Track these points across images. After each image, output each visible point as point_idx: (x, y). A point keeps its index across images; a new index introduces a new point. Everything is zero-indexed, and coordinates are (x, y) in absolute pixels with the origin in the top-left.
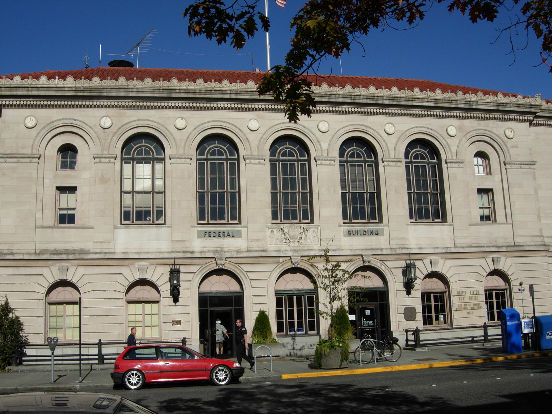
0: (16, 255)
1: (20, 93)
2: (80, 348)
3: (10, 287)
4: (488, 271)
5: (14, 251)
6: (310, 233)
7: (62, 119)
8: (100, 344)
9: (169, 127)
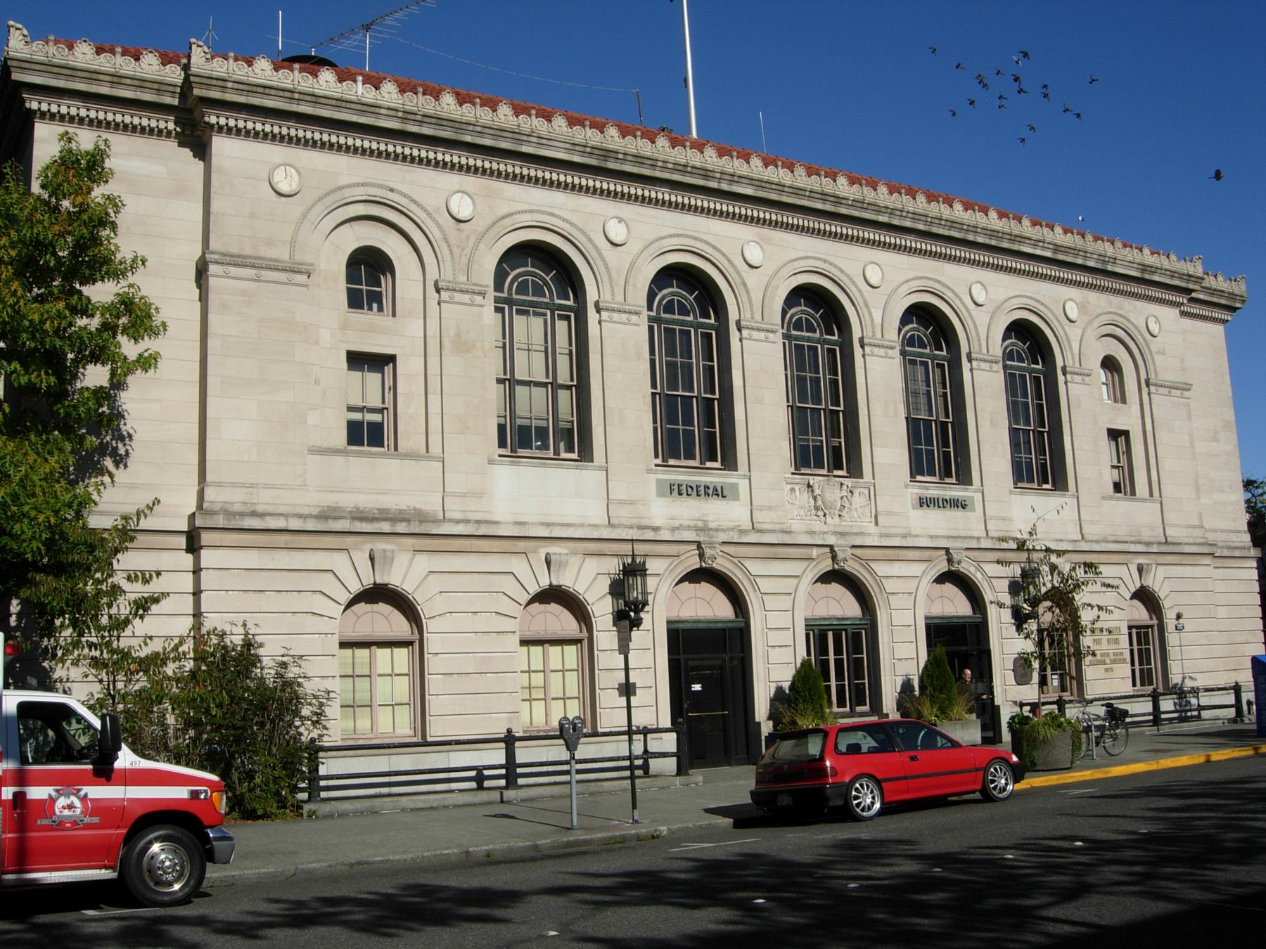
0: (268, 518)
1: (269, 103)
2: (630, 741)
3: (253, 602)
4: (534, 589)
5: (260, 509)
6: (858, 500)
7: (363, 185)
8: (509, 740)
9: (592, 235)
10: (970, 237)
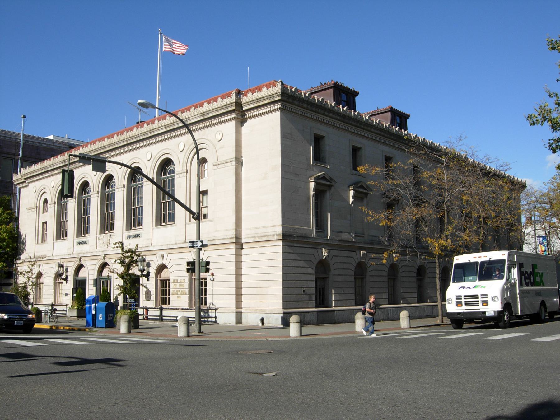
10: (139, 139)
